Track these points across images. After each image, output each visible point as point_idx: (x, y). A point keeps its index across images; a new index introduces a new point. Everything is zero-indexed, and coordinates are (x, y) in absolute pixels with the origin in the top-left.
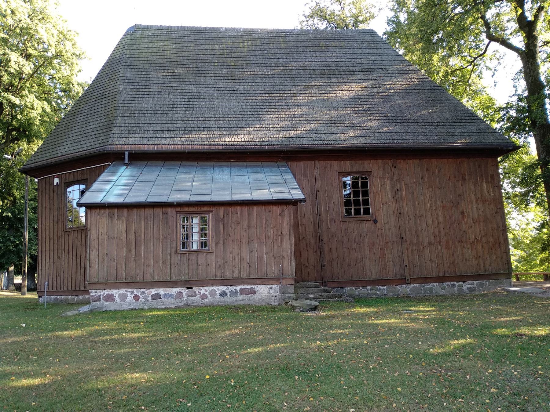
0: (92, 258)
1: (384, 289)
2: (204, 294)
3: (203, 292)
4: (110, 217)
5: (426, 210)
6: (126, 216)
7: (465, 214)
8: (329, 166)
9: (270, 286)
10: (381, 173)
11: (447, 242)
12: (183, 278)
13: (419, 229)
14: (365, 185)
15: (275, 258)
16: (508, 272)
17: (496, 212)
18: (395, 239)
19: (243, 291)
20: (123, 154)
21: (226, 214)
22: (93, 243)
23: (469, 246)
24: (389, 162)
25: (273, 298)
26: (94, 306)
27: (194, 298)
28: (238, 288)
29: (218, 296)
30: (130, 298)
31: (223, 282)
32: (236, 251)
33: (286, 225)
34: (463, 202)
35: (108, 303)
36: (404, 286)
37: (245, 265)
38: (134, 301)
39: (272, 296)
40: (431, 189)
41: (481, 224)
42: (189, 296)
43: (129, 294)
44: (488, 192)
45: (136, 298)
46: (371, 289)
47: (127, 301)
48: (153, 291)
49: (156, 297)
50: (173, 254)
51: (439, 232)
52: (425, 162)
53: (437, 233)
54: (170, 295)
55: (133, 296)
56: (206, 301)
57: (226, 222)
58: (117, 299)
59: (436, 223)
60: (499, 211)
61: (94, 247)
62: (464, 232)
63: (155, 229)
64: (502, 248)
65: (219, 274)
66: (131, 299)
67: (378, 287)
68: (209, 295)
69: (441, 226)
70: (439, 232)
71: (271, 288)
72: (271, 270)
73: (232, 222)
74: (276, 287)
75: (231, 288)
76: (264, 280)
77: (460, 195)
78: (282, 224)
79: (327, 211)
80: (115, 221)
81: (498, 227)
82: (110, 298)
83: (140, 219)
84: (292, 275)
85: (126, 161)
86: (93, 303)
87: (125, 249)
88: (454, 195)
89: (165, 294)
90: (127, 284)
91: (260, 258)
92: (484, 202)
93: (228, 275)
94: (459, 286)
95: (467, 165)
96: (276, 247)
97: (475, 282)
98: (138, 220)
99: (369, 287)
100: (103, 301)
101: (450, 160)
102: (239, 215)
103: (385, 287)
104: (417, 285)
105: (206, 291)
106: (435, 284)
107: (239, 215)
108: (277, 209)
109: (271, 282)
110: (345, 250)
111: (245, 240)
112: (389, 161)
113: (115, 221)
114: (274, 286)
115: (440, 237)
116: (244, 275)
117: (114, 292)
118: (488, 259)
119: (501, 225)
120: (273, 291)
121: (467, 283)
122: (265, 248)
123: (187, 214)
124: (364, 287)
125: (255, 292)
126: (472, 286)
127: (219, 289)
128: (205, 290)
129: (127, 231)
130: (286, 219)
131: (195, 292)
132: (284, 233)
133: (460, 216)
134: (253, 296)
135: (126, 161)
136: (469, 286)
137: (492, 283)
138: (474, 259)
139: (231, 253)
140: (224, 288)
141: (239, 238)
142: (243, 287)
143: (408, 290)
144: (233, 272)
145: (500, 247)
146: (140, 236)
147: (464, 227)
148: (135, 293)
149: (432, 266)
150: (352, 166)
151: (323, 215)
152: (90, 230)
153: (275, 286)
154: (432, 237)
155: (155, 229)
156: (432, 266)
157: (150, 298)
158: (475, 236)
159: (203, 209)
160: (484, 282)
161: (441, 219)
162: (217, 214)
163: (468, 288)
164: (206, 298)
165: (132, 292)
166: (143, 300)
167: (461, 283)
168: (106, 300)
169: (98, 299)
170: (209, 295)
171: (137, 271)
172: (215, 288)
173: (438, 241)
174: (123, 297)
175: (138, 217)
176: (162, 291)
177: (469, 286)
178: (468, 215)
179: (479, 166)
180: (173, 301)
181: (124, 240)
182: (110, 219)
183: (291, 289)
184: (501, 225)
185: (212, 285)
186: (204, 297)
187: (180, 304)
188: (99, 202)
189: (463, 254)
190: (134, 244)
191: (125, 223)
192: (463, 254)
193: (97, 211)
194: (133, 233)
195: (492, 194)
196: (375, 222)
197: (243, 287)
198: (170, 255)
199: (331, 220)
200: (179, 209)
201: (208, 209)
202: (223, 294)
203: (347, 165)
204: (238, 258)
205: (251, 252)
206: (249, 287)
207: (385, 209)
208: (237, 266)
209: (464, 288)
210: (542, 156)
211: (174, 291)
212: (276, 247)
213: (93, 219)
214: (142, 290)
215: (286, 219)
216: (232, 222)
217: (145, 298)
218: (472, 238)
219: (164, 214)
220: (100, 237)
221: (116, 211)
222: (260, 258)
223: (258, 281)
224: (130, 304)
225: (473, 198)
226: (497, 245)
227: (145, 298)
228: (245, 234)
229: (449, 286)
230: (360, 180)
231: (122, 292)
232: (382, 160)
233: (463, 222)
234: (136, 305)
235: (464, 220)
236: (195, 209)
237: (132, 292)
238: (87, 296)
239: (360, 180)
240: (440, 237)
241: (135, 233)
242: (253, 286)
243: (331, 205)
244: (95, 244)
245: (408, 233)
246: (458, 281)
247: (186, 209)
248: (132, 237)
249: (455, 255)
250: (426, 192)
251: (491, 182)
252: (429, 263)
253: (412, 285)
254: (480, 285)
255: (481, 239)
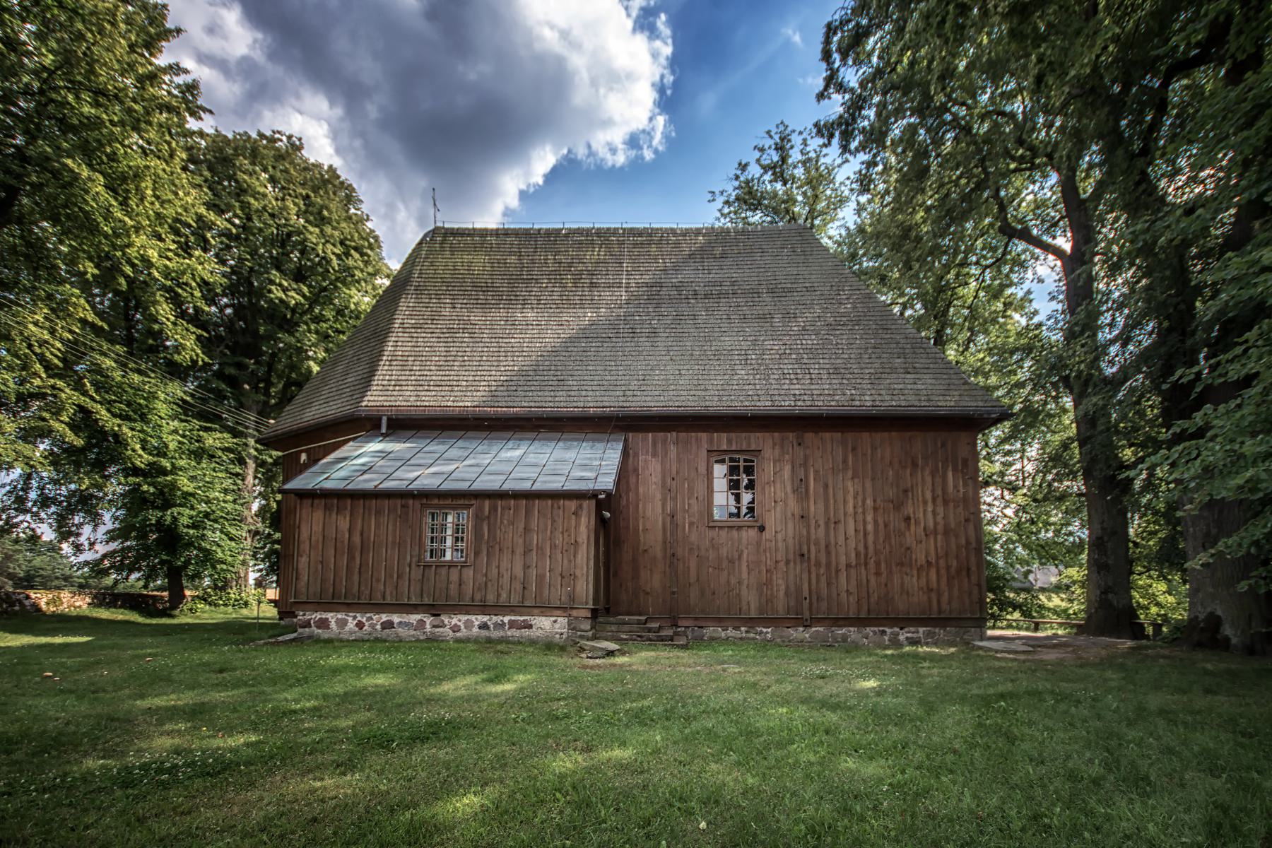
0: (301, 566)
1: (767, 633)
2: (456, 625)
3: (454, 621)
4: (327, 508)
5: (845, 514)
6: (349, 508)
7: (913, 521)
8: (693, 440)
9: (554, 619)
10: (777, 452)
11: (878, 564)
12: (426, 601)
13: (833, 542)
14: (749, 470)
15: (563, 577)
16: (978, 616)
17: (967, 520)
18: (791, 557)
19: (512, 624)
20: (380, 419)
21: (494, 509)
22: (302, 546)
23: (915, 572)
24: (791, 435)
25: (558, 636)
26: (300, 634)
27: (441, 629)
28: (506, 619)
29: (475, 630)
30: (351, 625)
31: (484, 608)
32: (505, 564)
33: (583, 529)
34: (910, 501)
35: (320, 631)
36: (801, 629)
37: (518, 586)
38: (357, 629)
39: (557, 633)
40: (856, 480)
41: (939, 537)
42: (434, 626)
43: (350, 619)
44: (955, 487)
45: (360, 625)
46: (747, 632)
47: (347, 628)
48: (384, 618)
49: (388, 625)
50: (413, 566)
51: (866, 548)
52: (850, 436)
53: (861, 548)
54: (408, 625)
55: (355, 622)
56: (458, 634)
57: (492, 521)
58: (333, 625)
59: (862, 533)
60: (972, 517)
61: (304, 551)
62: (908, 548)
63: (390, 527)
64: (973, 578)
65: (478, 596)
66: (352, 626)
67: (759, 629)
68: (462, 627)
69: (871, 538)
70: (866, 548)
71: (555, 622)
72: (557, 594)
73: (502, 522)
74: (563, 621)
75: (498, 619)
76: (545, 608)
77: (906, 491)
78: (578, 525)
79: (684, 510)
80: (334, 516)
81: (968, 543)
82: (323, 624)
83: (370, 515)
84: (587, 603)
85: (384, 431)
86: (300, 630)
87: (346, 555)
88: (895, 490)
89: (401, 622)
90: (349, 606)
91: (540, 578)
92: (946, 502)
93: (491, 599)
94: (891, 633)
95: (920, 442)
96: (566, 562)
97: (921, 630)
98: (366, 515)
99: (743, 629)
100: (314, 628)
101: (894, 433)
102: (512, 511)
103: (769, 630)
104: (821, 629)
105: (460, 621)
106: (852, 629)
107: (512, 511)
108: (572, 505)
109: (558, 612)
110: (711, 570)
111: (519, 550)
112: (791, 434)
113: (334, 516)
114: (560, 619)
115: (866, 555)
116: (515, 600)
117: (329, 615)
118: (946, 594)
119: (973, 540)
120: (557, 626)
121: (906, 630)
122: (548, 563)
123: (436, 508)
124: (737, 628)
125: (530, 627)
126: (915, 635)
127: (478, 619)
128: (458, 620)
129: (350, 531)
130: (584, 520)
131: (443, 621)
132: (580, 540)
133: (903, 524)
134: (526, 632)
135: (384, 431)
136: (909, 635)
137: (950, 632)
138: (921, 593)
139: (498, 567)
140: (485, 618)
141: (510, 546)
142: (513, 618)
143: (807, 635)
144: (499, 595)
145: (968, 575)
146: (369, 538)
147: (909, 540)
148: (359, 618)
149: (848, 601)
150: (729, 442)
151: (679, 517)
152: (299, 527)
153: (562, 619)
154: (853, 555)
155: (390, 527)
156: (848, 601)
157: (378, 627)
158: (926, 557)
159: (461, 502)
160: (937, 630)
161: (870, 527)
162: (481, 509)
163: (907, 638)
164: (459, 630)
165: (355, 618)
166: (370, 629)
167: (897, 629)
168: (318, 627)
169: (307, 624)
170: (462, 627)
171: (363, 588)
172: (473, 618)
173: (862, 561)
174: (342, 623)
175: (367, 511)
176: (396, 619)
177: (909, 635)
178: (917, 523)
179: (943, 445)
180: (412, 632)
181: (346, 541)
182: (327, 513)
183: (586, 625)
184: (973, 540)
185: (467, 613)
186: (456, 629)
187: (421, 638)
188: (497, 488)
189: (902, 584)
190: (359, 549)
191: (348, 518)
192: (902, 584)
193: (310, 501)
194: (358, 534)
195: (962, 490)
196: (762, 529)
197: (513, 618)
198: (410, 566)
199: (691, 524)
200: (424, 501)
201: (466, 502)
202: (484, 626)
203: (722, 440)
204: (507, 577)
205: (526, 567)
206: (522, 618)
207: (778, 509)
208: (505, 587)
209: (902, 638)
210: (1083, 430)
211: (414, 618)
212: (566, 562)
213: (304, 511)
214: (368, 615)
215: (584, 520)
216: (502, 522)
217: (372, 626)
218: (922, 559)
219: (403, 506)
220: (313, 538)
221: (550, 502)
222: (540, 578)
223: (536, 611)
224: (351, 633)
225: (929, 495)
226: (964, 573)
227: (372, 626)
228: (521, 541)
229: (875, 633)
230: (742, 464)
231: (340, 616)
232: (842, 432)
233: (907, 534)
234: (360, 634)
235: (909, 530)
236: (449, 502)
237: (355, 618)
238: (295, 620)
239: (742, 464)
240: (866, 555)
241: (362, 534)
242: (528, 618)
243: (693, 501)
244: (305, 547)
245: (813, 548)
246: (891, 627)
247: (436, 501)
248: (357, 539)
249: (889, 585)
250: (849, 484)
251: (962, 472)
252: (844, 595)
253: (814, 629)
254: (928, 635)
255: (937, 563)
